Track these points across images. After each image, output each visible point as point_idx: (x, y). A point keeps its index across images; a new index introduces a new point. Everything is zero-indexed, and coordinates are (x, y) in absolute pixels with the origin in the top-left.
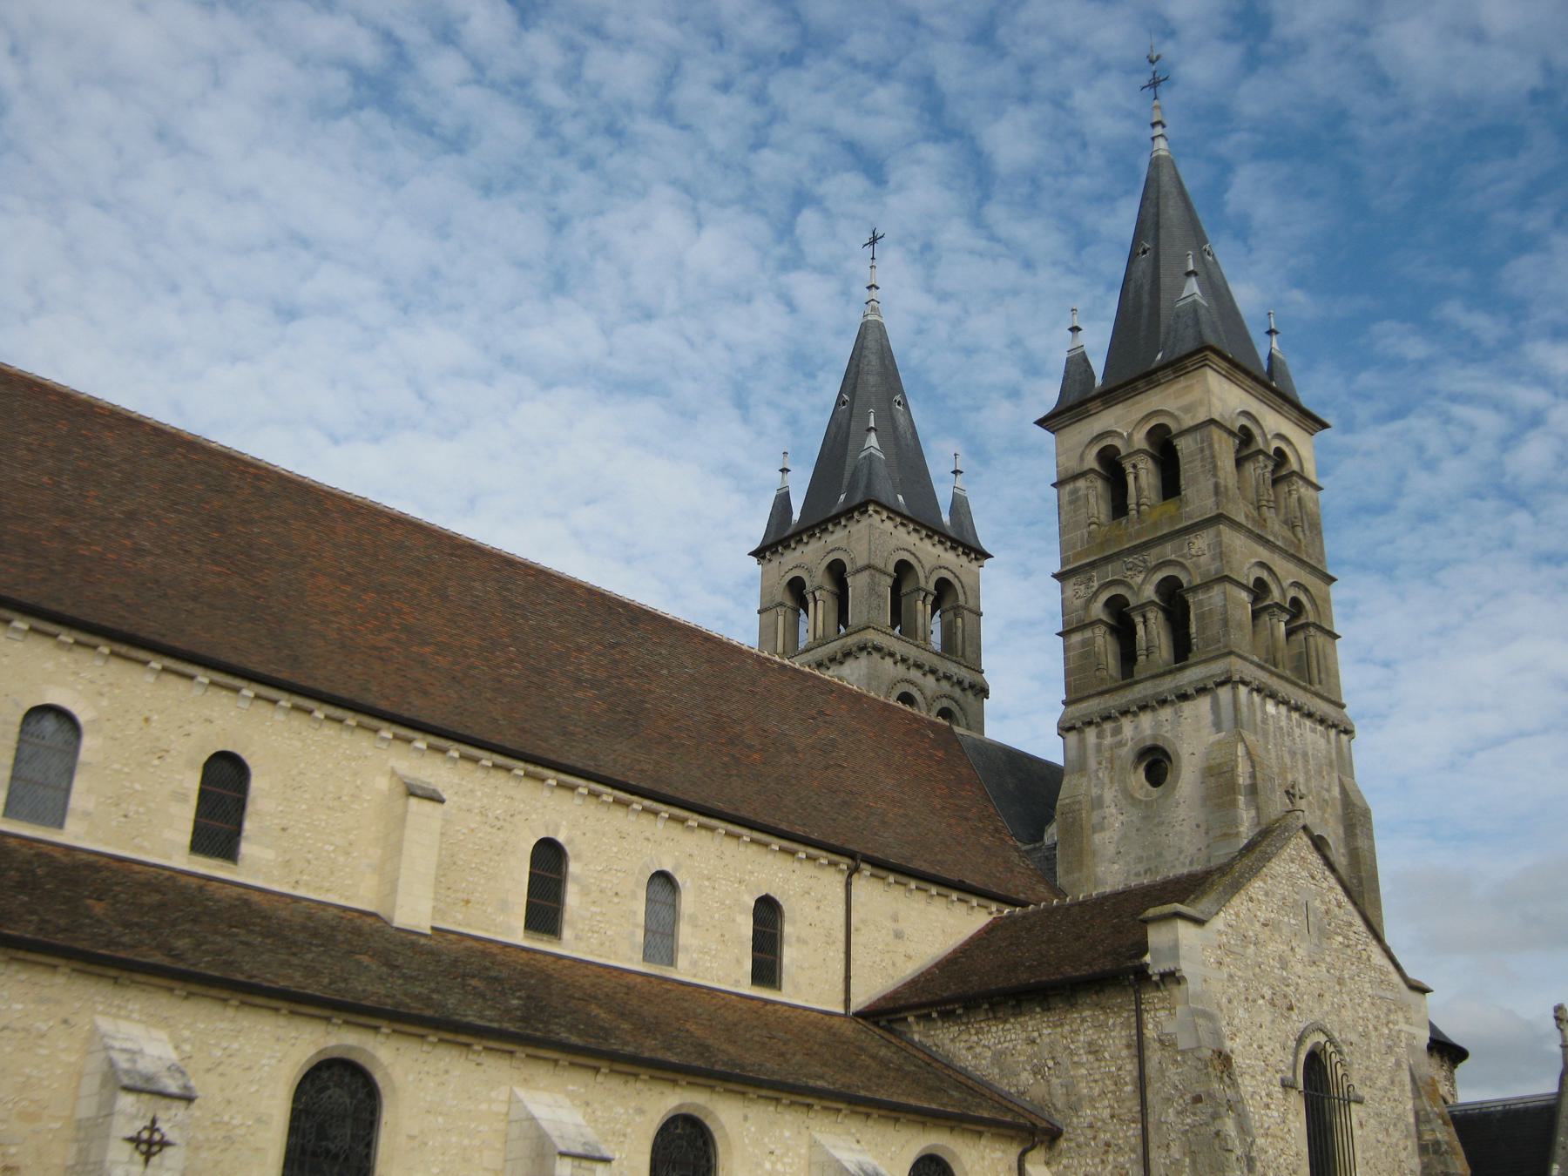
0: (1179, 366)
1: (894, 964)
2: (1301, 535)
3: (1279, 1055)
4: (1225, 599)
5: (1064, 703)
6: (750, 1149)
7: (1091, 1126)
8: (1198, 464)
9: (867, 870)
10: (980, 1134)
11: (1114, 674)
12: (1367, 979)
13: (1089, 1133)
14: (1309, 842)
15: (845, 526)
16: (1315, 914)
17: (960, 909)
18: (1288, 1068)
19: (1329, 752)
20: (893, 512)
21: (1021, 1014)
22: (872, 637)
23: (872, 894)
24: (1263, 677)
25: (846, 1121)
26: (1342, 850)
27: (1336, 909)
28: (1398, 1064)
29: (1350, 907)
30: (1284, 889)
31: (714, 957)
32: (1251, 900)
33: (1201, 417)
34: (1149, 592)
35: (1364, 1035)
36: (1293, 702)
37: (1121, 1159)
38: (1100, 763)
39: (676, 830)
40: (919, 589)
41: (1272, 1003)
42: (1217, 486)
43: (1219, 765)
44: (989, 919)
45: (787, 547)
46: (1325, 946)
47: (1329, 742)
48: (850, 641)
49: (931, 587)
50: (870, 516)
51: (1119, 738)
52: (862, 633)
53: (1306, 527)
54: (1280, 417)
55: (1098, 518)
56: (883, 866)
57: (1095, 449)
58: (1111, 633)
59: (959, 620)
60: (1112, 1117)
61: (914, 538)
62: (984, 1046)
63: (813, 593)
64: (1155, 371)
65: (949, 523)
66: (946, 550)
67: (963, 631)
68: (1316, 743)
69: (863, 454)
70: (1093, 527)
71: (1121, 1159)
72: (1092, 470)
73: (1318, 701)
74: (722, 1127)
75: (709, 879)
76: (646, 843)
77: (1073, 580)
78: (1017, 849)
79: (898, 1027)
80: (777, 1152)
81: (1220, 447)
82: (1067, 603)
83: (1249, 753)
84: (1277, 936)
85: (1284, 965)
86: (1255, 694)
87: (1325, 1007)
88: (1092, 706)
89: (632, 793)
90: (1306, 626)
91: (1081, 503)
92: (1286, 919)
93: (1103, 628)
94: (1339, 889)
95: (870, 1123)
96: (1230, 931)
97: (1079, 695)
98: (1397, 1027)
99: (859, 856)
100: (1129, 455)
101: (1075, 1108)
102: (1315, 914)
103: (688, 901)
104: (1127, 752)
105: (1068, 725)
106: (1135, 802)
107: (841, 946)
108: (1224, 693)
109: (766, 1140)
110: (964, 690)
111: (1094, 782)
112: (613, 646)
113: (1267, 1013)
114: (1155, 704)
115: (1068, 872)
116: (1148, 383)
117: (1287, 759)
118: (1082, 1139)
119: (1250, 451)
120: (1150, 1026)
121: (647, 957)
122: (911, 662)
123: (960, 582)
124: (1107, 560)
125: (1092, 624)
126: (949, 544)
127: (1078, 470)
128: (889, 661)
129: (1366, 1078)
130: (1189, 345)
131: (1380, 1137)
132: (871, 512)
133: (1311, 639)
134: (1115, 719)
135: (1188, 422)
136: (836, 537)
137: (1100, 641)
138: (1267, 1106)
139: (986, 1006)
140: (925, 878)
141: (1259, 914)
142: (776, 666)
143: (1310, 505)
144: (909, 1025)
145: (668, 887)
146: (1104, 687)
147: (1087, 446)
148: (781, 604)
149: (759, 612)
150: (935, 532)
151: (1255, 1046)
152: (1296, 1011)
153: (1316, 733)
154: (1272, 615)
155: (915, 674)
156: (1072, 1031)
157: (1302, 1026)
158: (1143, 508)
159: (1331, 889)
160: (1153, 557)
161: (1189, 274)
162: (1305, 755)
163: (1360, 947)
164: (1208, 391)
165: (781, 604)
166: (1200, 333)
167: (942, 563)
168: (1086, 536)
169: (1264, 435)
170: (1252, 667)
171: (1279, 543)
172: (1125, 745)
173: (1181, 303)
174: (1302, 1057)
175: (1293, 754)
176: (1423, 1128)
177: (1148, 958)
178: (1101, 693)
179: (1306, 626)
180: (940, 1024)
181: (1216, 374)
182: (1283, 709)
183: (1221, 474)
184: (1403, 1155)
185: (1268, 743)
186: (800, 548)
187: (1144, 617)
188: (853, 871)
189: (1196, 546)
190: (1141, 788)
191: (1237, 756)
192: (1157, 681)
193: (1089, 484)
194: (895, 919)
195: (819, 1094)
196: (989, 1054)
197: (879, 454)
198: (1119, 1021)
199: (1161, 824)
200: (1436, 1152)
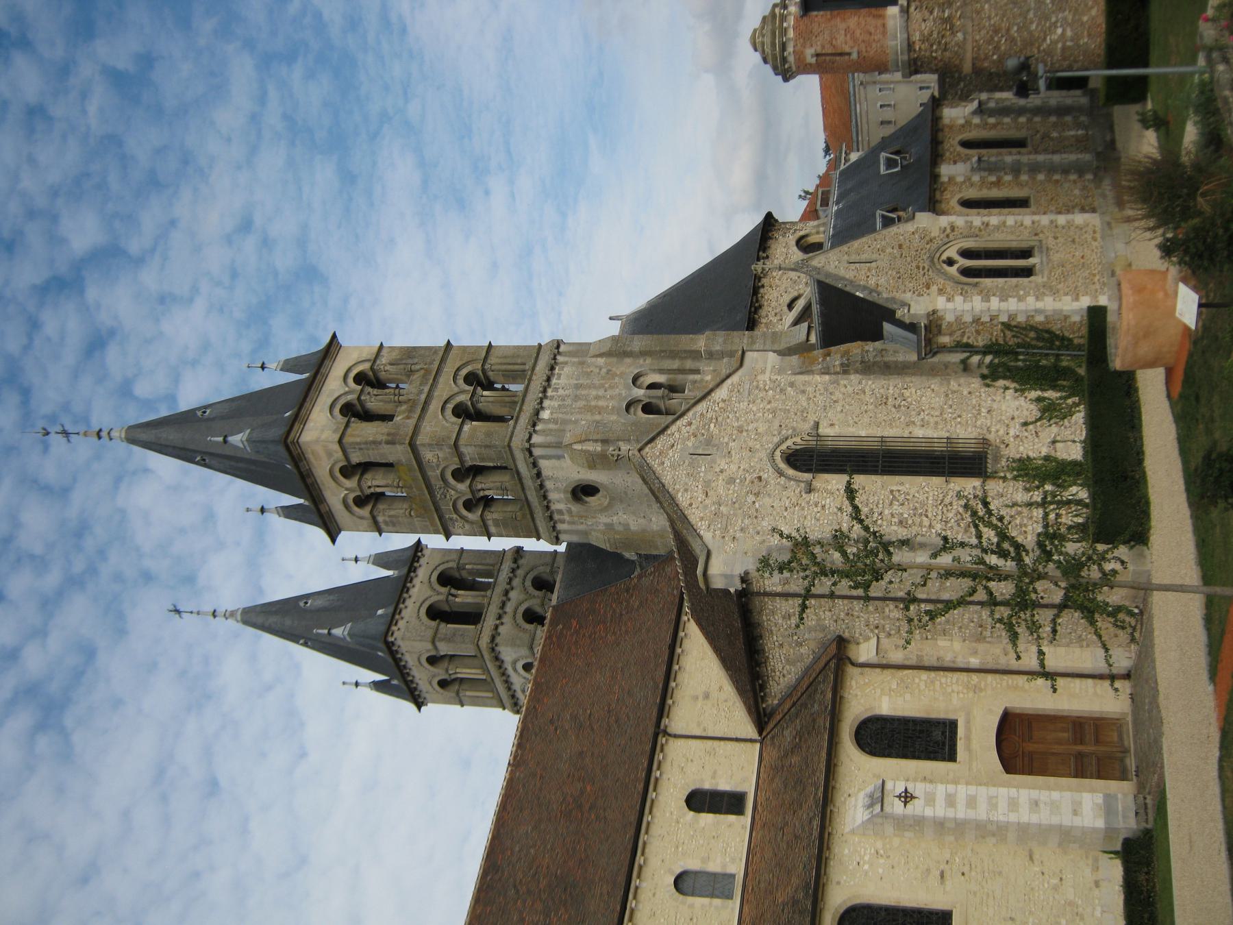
0: (297, 457)
1: (726, 701)
2: (418, 367)
3: (789, 493)
4: (471, 445)
5: (538, 539)
6: (857, 880)
7: (836, 621)
8: (371, 452)
9: (665, 721)
10: (841, 697)
11: (519, 507)
12: (737, 405)
13: (840, 622)
14: (649, 446)
15: (402, 654)
16: (697, 448)
17: (687, 644)
18: (799, 486)
19: (574, 364)
20: (392, 620)
21: (763, 650)
22: (484, 642)
23: (682, 717)
24: (524, 420)
25: (837, 805)
26: (641, 361)
27: (693, 427)
28: (792, 385)
29: (690, 414)
30: (682, 473)
31: (727, 844)
32: (691, 505)
33: (337, 447)
34: (463, 487)
35: (774, 412)
36: (540, 395)
37: (857, 609)
38: (582, 523)
39: (647, 872)
40: (447, 600)
41: (757, 494)
42: (388, 443)
43: (587, 461)
44: (692, 621)
45: (415, 689)
46: (717, 442)
47: (566, 363)
48: (487, 656)
49: (444, 590)
50: (395, 639)
51: (565, 512)
52: (482, 649)
53: (410, 361)
54: (330, 374)
55: (406, 509)
56: (662, 710)
57: (355, 509)
58: (489, 506)
59: (467, 567)
60: (830, 610)
61: (409, 602)
62: (783, 668)
63: (450, 675)
64: (300, 473)
65: (396, 572)
66: (416, 576)
67: (474, 564)
68: (568, 376)
69: (348, 639)
70: (412, 513)
71: (857, 609)
72: (371, 512)
73: (537, 368)
74: (844, 901)
75: (677, 847)
76: (657, 896)
77: (451, 528)
78: (640, 577)
79: (768, 711)
80: (858, 859)
81: (358, 436)
82: (468, 533)
83: (580, 442)
84: (713, 484)
85: (731, 481)
86: (537, 428)
87: (758, 447)
88: (542, 526)
89: (626, 908)
90: (483, 370)
91: (394, 519)
92: (702, 474)
93: (486, 513)
94: (679, 423)
95: (838, 786)
96: (712, 527)
97: (533, 530)
98: (768, 382)
99: (657, 730)
100: (362, 491)
101: (824, 628)
102: (697, 448)
103: (693, 865)
104: (575, 508)
105: (555, 540)
106: (610, 506)
107: (716, 743)
108: (537, 452)
109: (851, 867)
110: (518, 567)
111: (595, 527)
112: (517, 892)
113: (764, 500)
114: (542, 491)
115: (657, 548)
116: (309, 476)
117: (581, 403)
118: (844, 626)
119: (358, 405)
120: (774, 588)
121: (729, 896)
122: (501, 611)
123: (439, 565)
124: (437, 509)
125: (483, 520)
126: (412, 574)
127: (371, 521)
128: (501, 629)
129: (802, 415)
130: (281, 449)
131: (839, 409)
132: (393, 640)
133: (493, 368)
134: (552, 513)
135: (339, 454)
136: (410, 660)
137: (495, 516)
138: (823, 507)
139: (758, 669)
140: (668, 675)
141: (700, 499)
142: (519, 752)
143: (394, 355)
144: (768, 706)
145: (684, 877)
146: (529, 516)
147: (339, 485)
148: (458, 694)
149: (462, 706)
150: (404, 586)
151: (785, 514)
152: (761, 474)
153: (561, 374)
154: (478, 402)
155: (509, 608)
156: (776, 626)
157: (771, 470)
158: (401, 485)
159: (679, 430)
160: (437, 483)
161: (225, 441)
162: (578, 387)
163: (717, 409)
164: (317, 441)
165: (458, 694)
166: (273, 442)
167: (426, 580)
168: (419, 519)
169: (346, 393)
170: (518, 428)
171: (426, 389)
172: (570, 508)
173: (248, 449)
174: (791, 472)
175: (577, 398)
176: (832, 371)
177: (732, 590)
178: (533, 519)
179: (483, 370)
180: (768, 690)
181: (303, 433)
182: (546, 403)
183: (379, 438)
184: (850, 389)
185: (571, 420)
186: (417, 680)
187: (479, 490)
188: (666, 733)
189: (431, 458)
190: (599, 500)
191: (582, 450)
192: (527, 488)
193: (381, 514)
194: (696, 698)
195: (823, 827)
196: (788, 667)
197: (348, 628)
198: (770, 603)
199: (626, 493)
200: (848, 366)
